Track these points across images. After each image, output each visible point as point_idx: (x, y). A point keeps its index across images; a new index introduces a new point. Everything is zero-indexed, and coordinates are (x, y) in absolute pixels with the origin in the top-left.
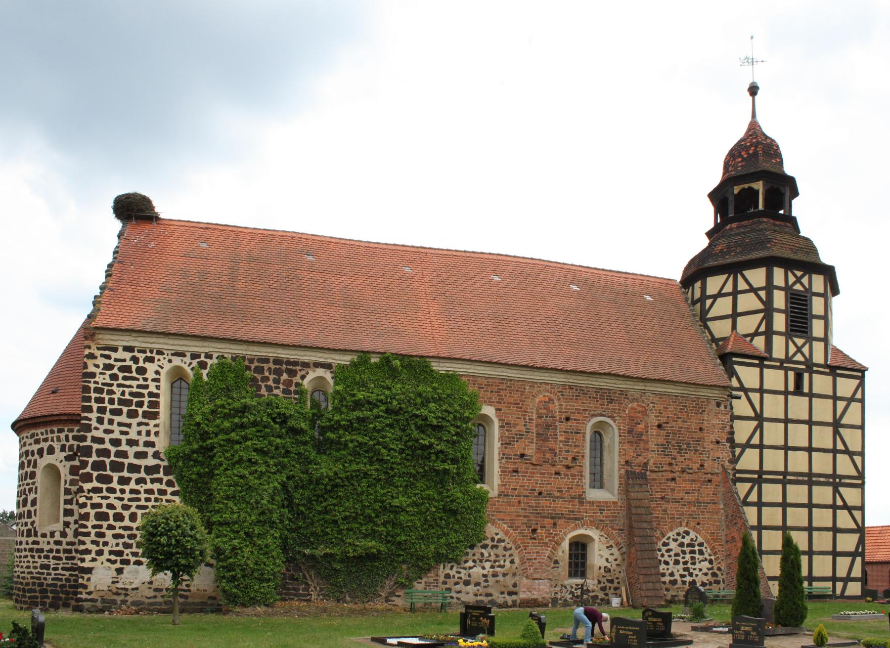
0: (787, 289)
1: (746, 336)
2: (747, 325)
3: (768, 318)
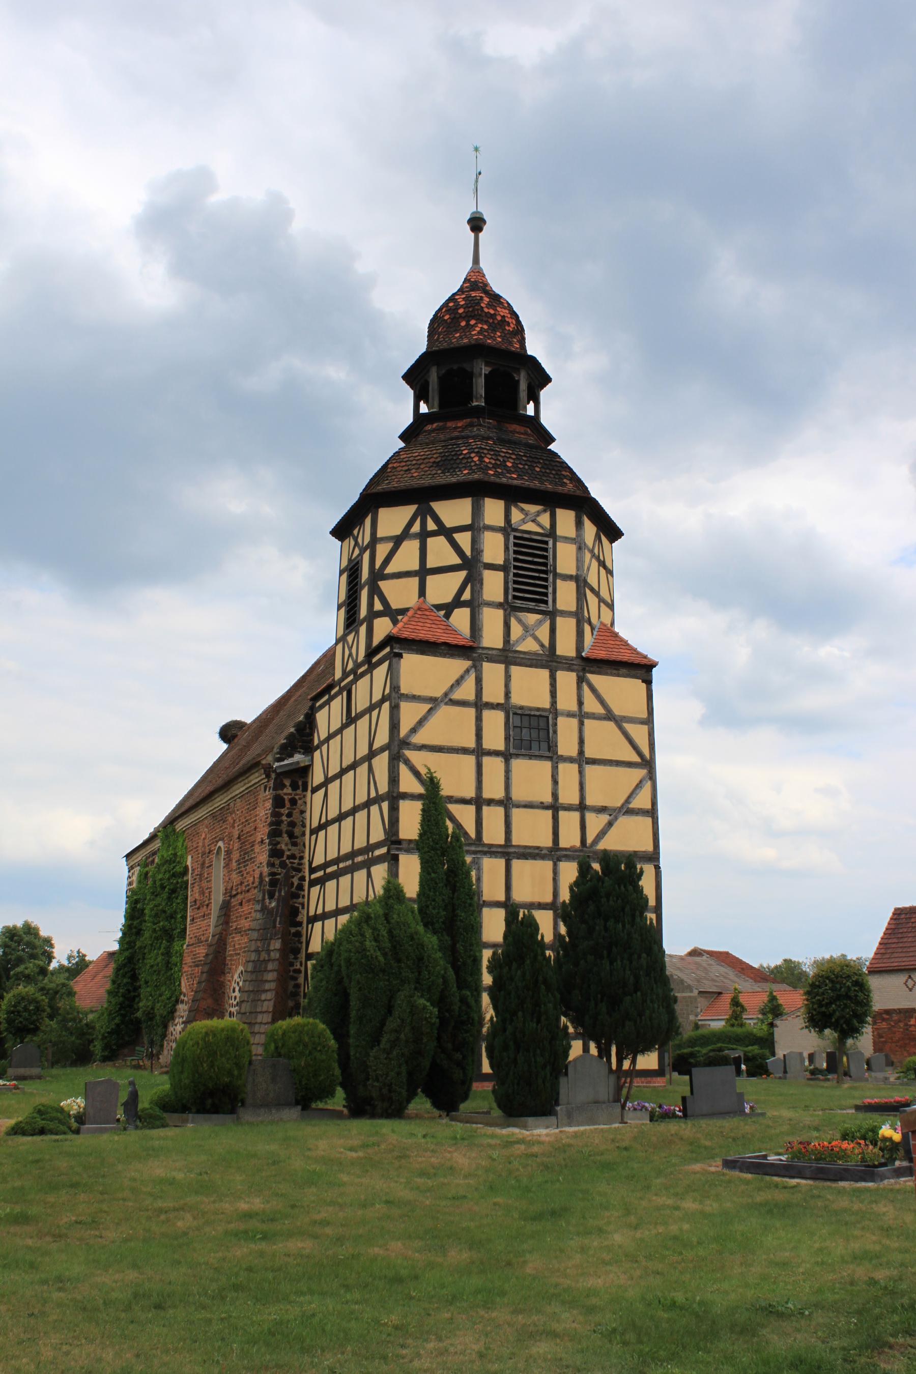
0: (507, 529)
1: (439, 607)
2: (442, 589)
3: (474, 579)
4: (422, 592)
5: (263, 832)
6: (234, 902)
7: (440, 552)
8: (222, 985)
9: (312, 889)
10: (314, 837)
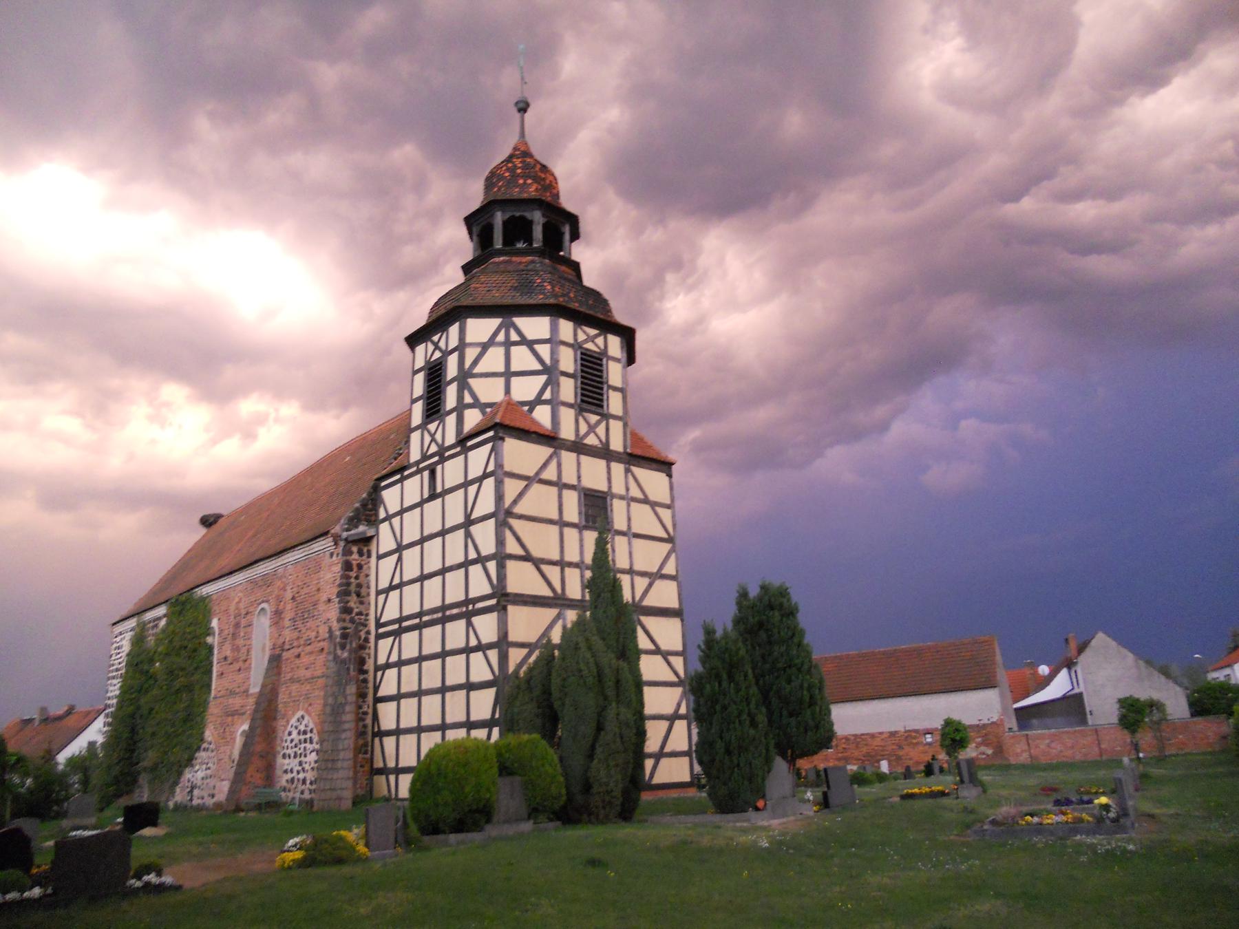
1: (523, 403)
4: (508, 391)
5: (331, 591)
6: (285, 655)
7: (522, 358)
8: (274, 731)
9: (381, 642)
10: (382, 598)
